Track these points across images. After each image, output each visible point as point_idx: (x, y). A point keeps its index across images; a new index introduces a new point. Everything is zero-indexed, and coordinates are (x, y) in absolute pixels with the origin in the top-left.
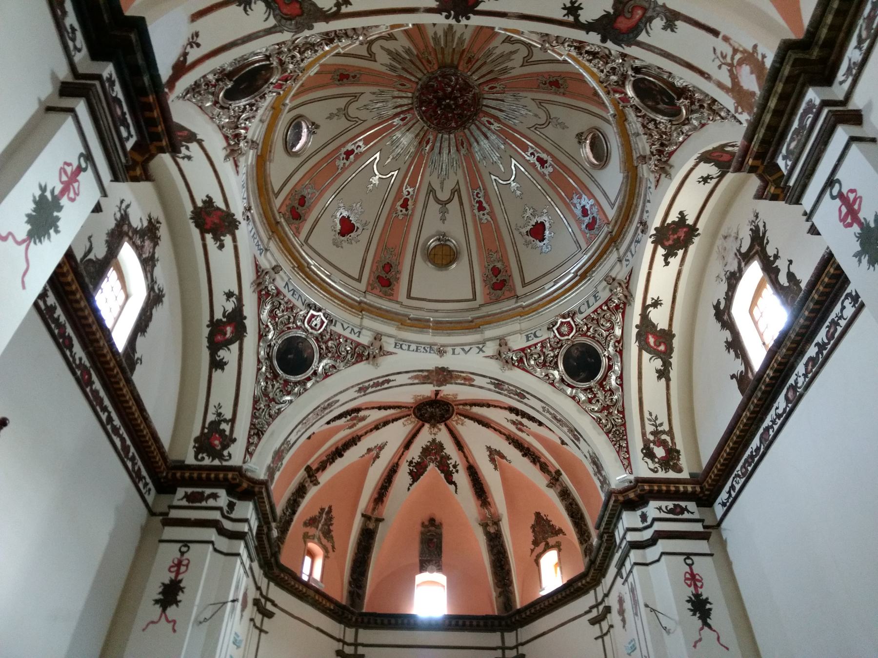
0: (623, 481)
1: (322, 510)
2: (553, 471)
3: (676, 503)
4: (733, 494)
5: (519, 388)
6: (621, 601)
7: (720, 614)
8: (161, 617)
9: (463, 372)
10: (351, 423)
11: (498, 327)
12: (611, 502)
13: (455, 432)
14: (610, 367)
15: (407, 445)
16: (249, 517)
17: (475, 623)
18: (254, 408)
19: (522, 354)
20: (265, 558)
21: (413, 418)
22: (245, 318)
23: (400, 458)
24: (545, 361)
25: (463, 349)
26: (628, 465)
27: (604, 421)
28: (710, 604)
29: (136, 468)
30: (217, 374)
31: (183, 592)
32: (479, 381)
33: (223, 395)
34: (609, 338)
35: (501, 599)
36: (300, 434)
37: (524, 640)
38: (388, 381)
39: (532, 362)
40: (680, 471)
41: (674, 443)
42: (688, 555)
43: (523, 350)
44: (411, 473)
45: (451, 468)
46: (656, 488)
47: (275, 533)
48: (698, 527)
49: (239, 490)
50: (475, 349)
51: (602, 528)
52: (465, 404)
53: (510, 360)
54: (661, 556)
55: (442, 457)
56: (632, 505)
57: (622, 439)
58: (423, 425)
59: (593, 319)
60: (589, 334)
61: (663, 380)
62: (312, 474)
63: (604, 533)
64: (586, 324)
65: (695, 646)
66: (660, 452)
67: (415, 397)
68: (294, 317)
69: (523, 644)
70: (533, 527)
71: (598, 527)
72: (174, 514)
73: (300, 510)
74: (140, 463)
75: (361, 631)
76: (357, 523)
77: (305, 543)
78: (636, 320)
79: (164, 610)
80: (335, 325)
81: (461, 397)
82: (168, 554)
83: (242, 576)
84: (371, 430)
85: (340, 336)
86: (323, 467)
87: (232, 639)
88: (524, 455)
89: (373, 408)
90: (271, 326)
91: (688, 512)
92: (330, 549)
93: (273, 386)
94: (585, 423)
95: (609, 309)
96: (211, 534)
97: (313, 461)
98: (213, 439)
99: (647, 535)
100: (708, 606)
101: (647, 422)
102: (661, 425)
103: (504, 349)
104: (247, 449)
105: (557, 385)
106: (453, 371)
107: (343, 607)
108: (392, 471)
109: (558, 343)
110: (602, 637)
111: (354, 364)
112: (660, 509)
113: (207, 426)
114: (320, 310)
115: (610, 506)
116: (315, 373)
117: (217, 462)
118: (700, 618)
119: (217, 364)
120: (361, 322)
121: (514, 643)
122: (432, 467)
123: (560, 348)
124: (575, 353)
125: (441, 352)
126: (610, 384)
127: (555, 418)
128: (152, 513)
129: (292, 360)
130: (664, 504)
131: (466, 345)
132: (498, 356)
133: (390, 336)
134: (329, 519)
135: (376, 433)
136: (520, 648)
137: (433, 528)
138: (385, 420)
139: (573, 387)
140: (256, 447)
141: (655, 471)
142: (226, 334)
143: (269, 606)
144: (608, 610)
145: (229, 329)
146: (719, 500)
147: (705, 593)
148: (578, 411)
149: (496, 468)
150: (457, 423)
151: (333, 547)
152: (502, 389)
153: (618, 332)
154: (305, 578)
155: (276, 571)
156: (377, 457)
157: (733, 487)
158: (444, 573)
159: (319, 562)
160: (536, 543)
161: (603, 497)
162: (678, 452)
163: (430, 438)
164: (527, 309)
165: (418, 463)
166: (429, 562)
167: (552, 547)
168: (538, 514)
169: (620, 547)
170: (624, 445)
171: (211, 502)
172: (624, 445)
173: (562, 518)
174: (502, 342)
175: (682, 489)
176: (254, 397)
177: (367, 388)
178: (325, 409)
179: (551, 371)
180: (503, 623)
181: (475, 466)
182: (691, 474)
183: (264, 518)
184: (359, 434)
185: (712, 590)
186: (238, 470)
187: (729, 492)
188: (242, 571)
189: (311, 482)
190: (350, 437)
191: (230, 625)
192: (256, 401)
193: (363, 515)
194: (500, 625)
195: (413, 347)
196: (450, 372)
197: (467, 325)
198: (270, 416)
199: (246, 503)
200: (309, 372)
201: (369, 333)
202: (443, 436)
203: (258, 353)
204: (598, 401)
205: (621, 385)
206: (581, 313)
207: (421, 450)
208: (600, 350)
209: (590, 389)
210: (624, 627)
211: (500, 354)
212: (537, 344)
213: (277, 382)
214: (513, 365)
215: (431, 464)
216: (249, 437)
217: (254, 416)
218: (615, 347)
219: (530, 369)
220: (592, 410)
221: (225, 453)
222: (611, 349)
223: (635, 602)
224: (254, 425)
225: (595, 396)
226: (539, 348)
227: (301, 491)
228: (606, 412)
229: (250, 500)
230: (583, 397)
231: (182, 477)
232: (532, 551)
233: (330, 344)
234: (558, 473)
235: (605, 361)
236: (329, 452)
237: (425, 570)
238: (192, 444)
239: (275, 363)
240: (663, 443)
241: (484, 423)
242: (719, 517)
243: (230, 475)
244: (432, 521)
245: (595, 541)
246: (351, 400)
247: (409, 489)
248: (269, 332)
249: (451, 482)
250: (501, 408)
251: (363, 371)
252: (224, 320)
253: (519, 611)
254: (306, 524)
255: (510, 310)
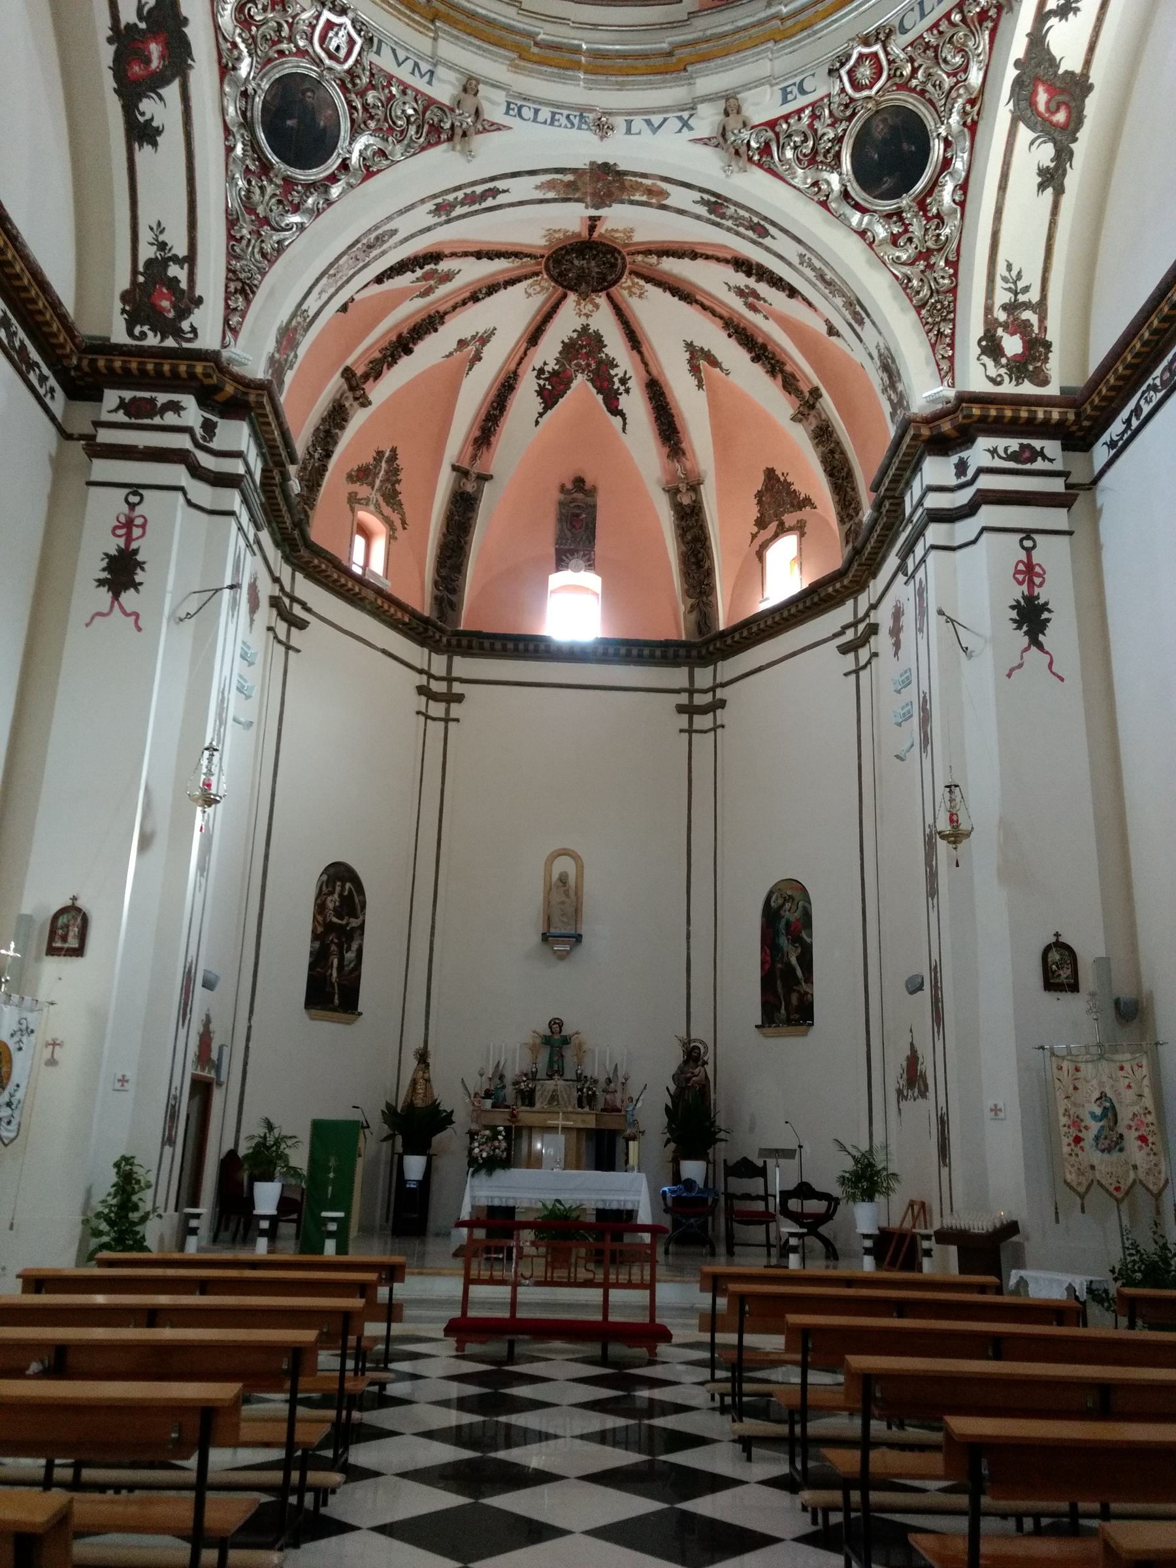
0: (933, 400)
1: (380, 454)
2: (805, 389)
3: (1025, 441)
4: (1135, 423)
5: (757, 214)
6: (898, 614)
7: (1061, 631)
8: (112, 607)
9: (644, 176)
10: (424, 285)
11: (726, 68)
12: (907, 439)
13: (627, 312)
14: (946, 163)
15: (534, 337)
16: (243, 448)
17: (646, 652)
18: (230, 237)
19: (770, 134)
20: (282, 530)
21: (544, 280)
22: (185, 21)
23: (519, 364)
24: (815, 151)
25: (649, 122)
26: (947, 369)
27: (915, 283)
28: (1050, 611)
29: (17, 344)
30: (144, 154)
31: (143, 569)
32: (678, 197)
33: (163, 205)
34: (953, 94)
35: (693, 617)
36: (325, 297)
37: (726, 679)
38: (494, 193)
39: (789, 154)
40: (1044, 382)
41: (1043, 328)
42: (1028, 533)
43: (772, 124)
44: (541, 392)
45: (617, 385)
46: (993, 413)
47: (295, 486)
48: (1056, 485)
49: (220, 397)
50: (674, 124)
51: (882, 489)
52: (648, 252)
53: (743, 149)
54: (981, 533)
55: (600, 362)
56: (941, 445)
57: (944, 320)
58: (565, 296)
59: (928, 46)
60: (914, 82)
61: (1049, 191)
62: (356, 384)
63: (885, 497)
64: (911, 60)
65: (1009, 676)
66: (1012, 345)
67: (550, 232)
68: (291, 26)
69: (723, 685)
70: (759, 495)
71: (875, 488)
72: (105, 436)
73: (339, 450)
74: (21, 334)
75: (457, 660)
76: (445, 482)
77: (353, 510)
78: (1018, 47)
79: (116, 596)
80: (378, 52)
81: (641, 237)
82: (107, 507)
83: (241, 551)
84: (464, 303)
85: (390, 78)
86: (375, 371)
87: (238, 652)
88: (756, 359)
89: (466, 254)
90: (242, 46)
91: (1044, 457)
92: (398, 524)
93: (262, 188)
94: (878, 287)
95: (964, 20)
96: (178, 474)
97: (357, 358)
98: (157, 292)
99: (963, 497)
100: (1045, 615)
101: (999, 283)
102: (1026, 289)
103: (733, 122)
104: (226, 321)
105: (833, 205)
106: (626, 173)
107: (426, 621)
108: (506, 387)
109: (847, 106)
110: (856, 672)
111: (423, 149)
112: (993, 452)
113: (141, 269)
114: (343, 11)
115: (904, 447)
116: (345, 166)
117: (170, 342)
118: (1026, 633)
119: (142, 133)
120: (435, 48)
121: (709, 684)
122: (580, 383)
123: (850, 119)
124: (879, 130)
125: (602, 128)
126: (940, 202)
127: (822, 277)
128: (65, 435)
129: (293, 131)
130: (1001, 443)
131: (654, 111)
132: (720, 139)
133: (495, 85)
134: (394, 473)
135: (473, 309)
136: (718, 691)
137: (580, 496)
138: (490, 282)
139: (864, 211)
140: (243, 317)
141: (996, 382)
142: (148, 61)
143: (297, 610)
144: (873, 629)
145: (155, 49)
146: (1105, 438)
147: (1044, 594)
148: (869, 262)
149: (700, 386)
150: (631, 294)
151: (404, 523)
152: (723, 216)
153: (975, 77)
154: (357, 570)
155: (304, 552)
156: (477, 358)
157: (1137, 411)
158: (597, 574)
159: (379, 546)
160: (761, 523)
161: (892, 431)
162: (1048, 346)
163: (578, 323)
164: (789, 23)
165: (554, 373)
166: (572, 552)
167: (790, 530)
168: (770, 473)
169: (910, 520)
170: (948, 331)
171: (170, 418)
172: (948, 331)
173: (813, 480)
174: (731, 104)
175: (1040, 415)
176: (227, 211)
177: (452, 206)
178: (370, 247)
179: (826, 175)
180: (694, 653)
181: (661, 381)
182: (1062, 389)
183: (276, 452)
184: (442, 309)
185: (1057, 592)
186: (211, 357)
187: (1128, 422)
188: (242, 543)
189: (356, 399)
190: (423, 315)
191: (232, 627)
192: (232, 222)
193: (455, 468)
194: (688, 656)
195: (545, 114)
196: (621, 174)
197: (660, 61)
198: (264, 255)
199: (238, 423)
200: (333, 163)
201: (452, 76)
202: (604, 321)
203: (223, 111)
204: (910, 240)
205: (962, 204)
206: (904, 31)
207: (560, 347)
208: (930, 123)
209: (898, 214)
210: (896, 654)
211: (723, 135)
212: (802, 110)
213: (271, 181)
214: (750, 159)
215: (580, 376)
216: (227, 299)
217: (232, 255)
218: (965, 113)
219: (781, 169)
220: (897, 261)
221: (185, 325)
222: (955, 119)
223: (922, 611)
224: (234, 272)
225: (906, 231)
226: (806, 120)
227: (337, 416)
228: (922, 264)
229: (244, 420)
230: (881, 231)
231: (110, 369)
232: (754, 536)
233: (371, 97)
234: (815, 393)
235: (937, 150)
236: (384, 343)
237: (567, 567)
238: (118, 305)
239: (261, 136)
240: (1022, 328)
241: (683, 293)
242: (1098, 466)
243: (199, 369)
244: (579, 482)
245: (866, 514)
246: (422, 232)
247: (537, 423)
248: (239, 59)
249: (615, 411)
250: (718, 260)
251: (440, 168)
252: (143, 26)
253: (723, 635)
254: (351, 478)
255: (753, 25)
